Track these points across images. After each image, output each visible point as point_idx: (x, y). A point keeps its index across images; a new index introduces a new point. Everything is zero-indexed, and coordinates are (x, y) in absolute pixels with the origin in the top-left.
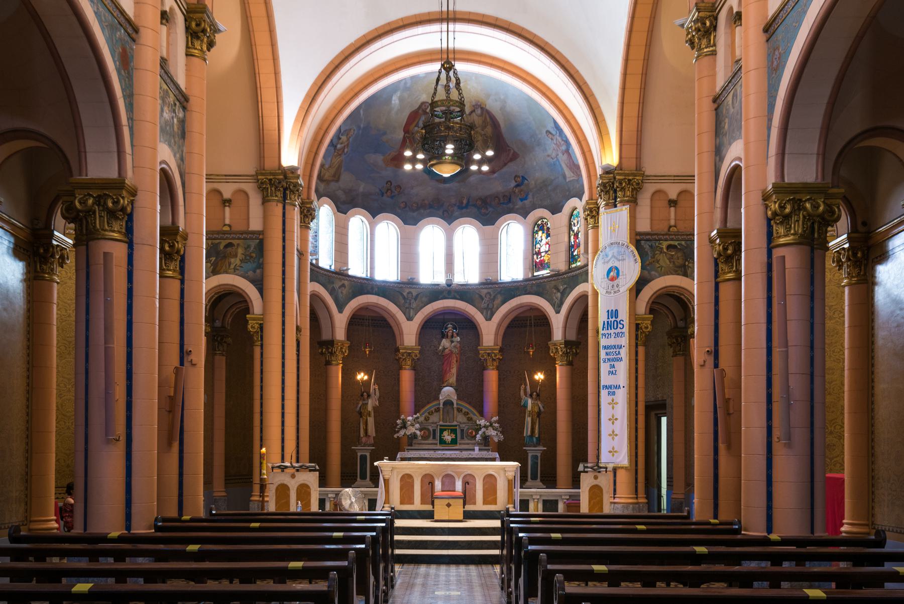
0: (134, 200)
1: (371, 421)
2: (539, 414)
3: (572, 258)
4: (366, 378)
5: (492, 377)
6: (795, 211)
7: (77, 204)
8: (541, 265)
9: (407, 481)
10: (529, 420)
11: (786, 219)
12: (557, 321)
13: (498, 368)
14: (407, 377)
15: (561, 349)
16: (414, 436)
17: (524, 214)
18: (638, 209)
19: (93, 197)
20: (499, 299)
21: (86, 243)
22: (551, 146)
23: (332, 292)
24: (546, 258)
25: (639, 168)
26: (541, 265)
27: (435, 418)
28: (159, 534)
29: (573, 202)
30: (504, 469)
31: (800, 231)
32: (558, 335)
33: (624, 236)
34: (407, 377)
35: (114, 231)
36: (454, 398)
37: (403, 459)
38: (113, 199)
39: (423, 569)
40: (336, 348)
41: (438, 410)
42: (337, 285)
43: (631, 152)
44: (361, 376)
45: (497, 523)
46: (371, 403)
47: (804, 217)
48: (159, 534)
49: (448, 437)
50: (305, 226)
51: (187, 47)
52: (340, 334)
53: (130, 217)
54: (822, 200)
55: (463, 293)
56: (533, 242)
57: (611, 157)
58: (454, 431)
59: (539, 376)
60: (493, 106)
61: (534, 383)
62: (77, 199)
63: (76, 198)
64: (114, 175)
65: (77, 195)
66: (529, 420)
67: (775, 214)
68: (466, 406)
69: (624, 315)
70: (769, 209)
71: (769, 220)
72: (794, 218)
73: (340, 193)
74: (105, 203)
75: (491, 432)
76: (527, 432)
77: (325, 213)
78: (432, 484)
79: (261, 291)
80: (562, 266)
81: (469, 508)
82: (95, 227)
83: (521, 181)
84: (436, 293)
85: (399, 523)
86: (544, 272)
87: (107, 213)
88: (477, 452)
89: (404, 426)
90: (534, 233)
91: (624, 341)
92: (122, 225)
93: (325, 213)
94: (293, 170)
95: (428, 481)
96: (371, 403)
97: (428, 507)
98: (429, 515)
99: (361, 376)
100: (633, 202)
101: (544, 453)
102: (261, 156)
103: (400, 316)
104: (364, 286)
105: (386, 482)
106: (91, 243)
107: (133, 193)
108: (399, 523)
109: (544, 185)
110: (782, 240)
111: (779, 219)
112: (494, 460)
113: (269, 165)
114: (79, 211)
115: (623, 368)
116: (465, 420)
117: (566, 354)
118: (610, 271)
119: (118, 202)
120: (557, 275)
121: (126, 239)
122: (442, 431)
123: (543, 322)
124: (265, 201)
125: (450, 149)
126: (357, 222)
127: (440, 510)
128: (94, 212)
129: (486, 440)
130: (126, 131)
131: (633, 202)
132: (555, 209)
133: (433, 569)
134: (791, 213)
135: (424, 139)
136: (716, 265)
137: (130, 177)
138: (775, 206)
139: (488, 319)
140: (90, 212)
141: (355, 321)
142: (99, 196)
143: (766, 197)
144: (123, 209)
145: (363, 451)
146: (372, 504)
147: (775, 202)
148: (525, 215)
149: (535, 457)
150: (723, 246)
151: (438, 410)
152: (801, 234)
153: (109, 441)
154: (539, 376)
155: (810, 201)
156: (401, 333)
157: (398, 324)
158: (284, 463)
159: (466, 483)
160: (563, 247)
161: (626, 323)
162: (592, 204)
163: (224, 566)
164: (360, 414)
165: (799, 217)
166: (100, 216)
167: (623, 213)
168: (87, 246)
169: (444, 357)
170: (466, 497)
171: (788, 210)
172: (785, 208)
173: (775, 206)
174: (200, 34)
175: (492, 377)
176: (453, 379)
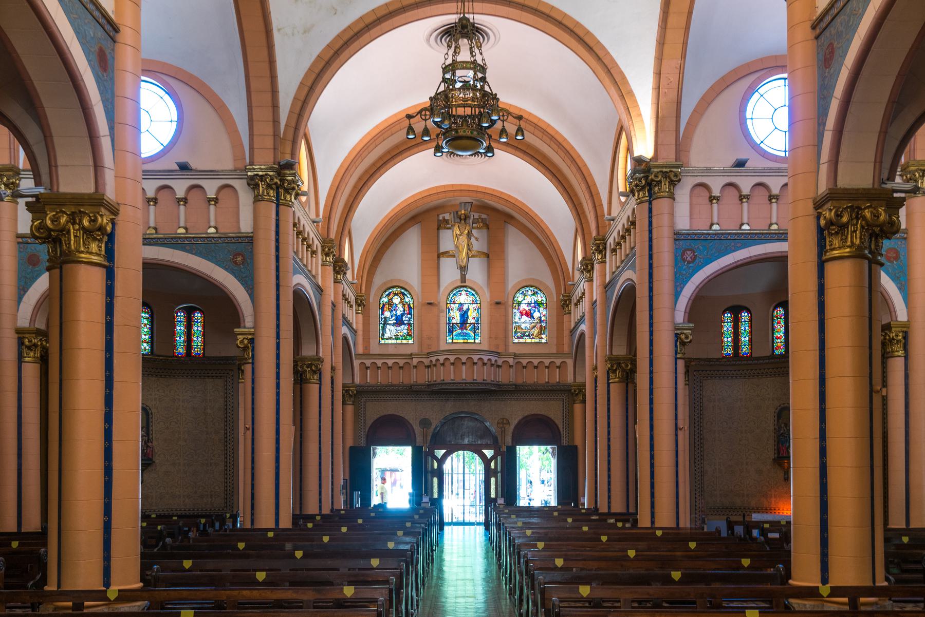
0: (115, 219)
6: (852, 220)
7: (299, 368)
11: (614, 371)
19: (67, 214)
21: (59, 266)
31: (857, 243)
35: (91, 253)
38: (90, 217)
47: (862, 227)
51: (334, 279)
53: (111, 237)
54: (883, 208)
62: (49, 216)
63: (47, 215)
65: (48, 212)
67: (830, 223)
70: (822, 218)
71: (820, 231)
72: (851, 228)
74: (81, 222)
82: (69, 247)
87: (84, 233)
92: (101, 247)
106: (66, 267)
107: (114, 211)
110: (836, 253)
111: (834, 229)
114: (50, 230)
118: (507, 420)
119: (95, 220)
121: (106, 263)
128: (69, 232)
130: (105, 143)
134: (848, 222)
136: (608, 374)
137: (110, 193)
138: (830, 214)
140: (64, 231)
142: (73, 213)
143: (818, 205)
144: (101, 229)
147: (831, 210)
150: (836, 212)
152: (858, 246)
155: (870, 209)
162: (599, 239)
165: (857, 228)
166: (75, 236)
168: (61, 268)
171: (845, 219)
172: (842, 217)
173: (830, 214)
174: (290, 191)
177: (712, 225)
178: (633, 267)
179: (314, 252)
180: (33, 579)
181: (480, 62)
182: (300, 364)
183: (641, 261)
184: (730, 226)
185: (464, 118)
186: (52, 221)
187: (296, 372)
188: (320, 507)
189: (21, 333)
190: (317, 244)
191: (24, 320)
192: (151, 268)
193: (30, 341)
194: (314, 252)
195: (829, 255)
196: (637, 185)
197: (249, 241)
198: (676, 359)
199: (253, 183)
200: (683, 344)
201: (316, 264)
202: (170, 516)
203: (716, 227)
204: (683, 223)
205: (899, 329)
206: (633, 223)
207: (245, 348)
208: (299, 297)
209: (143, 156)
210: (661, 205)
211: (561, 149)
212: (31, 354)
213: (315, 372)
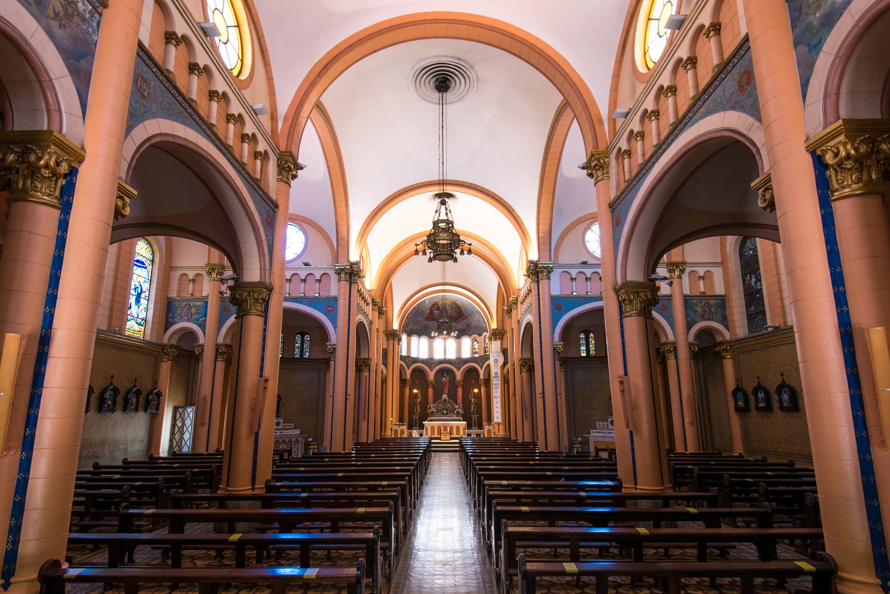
1: (418, 406)
2: (476, 403)
3: (486, 352)
4: (417, 391)
5: (460, 390)
8: (476, 353)
9: (433, 428)
10: (472, 406)
12: (481, 372)
13: (462, 387)
14: (430, 391)
15: (483, 381)
16: (433, 411)
17: (470, 336)
18: (504, 341)
20: (462, 364)
22: (477, 315)
23: (406, 363)
24: (477, 350)
25: (503, 329)
26: (476, 353)
27: (440, 405)
28: (125, 465)
29: (485, 333)
30: (462, 424)
32: (482, 377)
33: (499, 350)
34: (430, 391)
36: (447, 399)
37: (430, 421)
39: (438, 453)
40: (407, 382)
41: (441, 402)
42: (407, 360)
43: (501, 324)
44: (415, 391)
45: (458, 441)
46: (419, 400)
47: (640, 301)
48: (125, 465)
49: (445, 412)
50: (399, 344)
52: (408, 377)
55: (449, 362)
56: (473, 345)
57: (494, 326)
58: (447, 410)
59: (476, 391)
60: (458, 302)
61: (474, 393)
64: (367, 357)
66: (472, 406)
68: (451, 401)
69: (499, 374)
71: (620, 303)
73: (409, 331)
75: (460, 410)
76: (472, 410)
77: (404, 337)
78: (440, 429)
79: (386, 367)
80: (483, 354)
81: (452, 436)
83: (469, 325)
84: (441, 362)
85: (433, 441)
86: (477, 356)
88: (455, 417)
89: (430, 408)
90: (473, 342)
91: (499, 382)
93: (404, 337)
94: (396, 330)
95: (439, 428)
96: (419, 400)
97: (439, 436)
98: (440, 439)
99: (415, 391)
100: (502, 339)
101: (478, 417)
102: (387, 326)
103: (428, 370)
104: (416, 360)
105: (426, 429)
106: (361, 373)
108: (433, 441)
109: (476, 327)
112: (460, 420)
113: (389, 329)
114: (238, 300)
115: (499, 391)
116: (451, 406)
117: (485, 383)
120: (481, 357)
122: (443, 410)
123: (476, 371)
124: (388, 340)
125: (445, 332)
126: (414, 339)
127: (443, 437)
128: (247, 301)
129: (458, 413)
131: (502, 339)
132: (480, 335)
133: (441, 453)
135: (438, 328)
139: (458, 370)
140: (361, 365)
141: (414, 371)
142: (249, 292)
145: (416, 417)
146: (421, 435)
148: (470, 336)
149: (475, 419)
151: (441, 402)
153: (364, 420)
154: (476, 391)
156: (429, 376)
157: (428, 373)
158: (668, 507)
159: (450, 429)
160: (483, 348)
161: (500, 376)
163: (178, 512)
164: (415, 404)
167: (499, 342)
169: (443, 384)
170: (451, 433)
175: (460, 390)
176: (446, 392)
177: (573, 292)
178: (530, 313)
179: (368, 304)
180: (192, 471)
181: (450, 219)
182: (359, 361)
183: (535, 310)
184: (582, 293)
185: (443, 244)
186: (239, 295)
187: (357, 365)
188: (368, 439)
189: (218, 347)
190: (370, 300)
191: (220, 340)
192: (287, 312)
193: (222, 350)
194: (368, 304)
195: (625, 315)
196: (531, 273)
197: (335, 299)
198: (555, 360)
199: (338, 272)
200: (558, 353)
201: (369, 310)
202: (496, 575)
203: (574, 294)
204: (556, 291)
205: (671, 345)
206: (530, 291)
207: (332, 353)
208: (361, 325)
209: (286, 260)
210: (543, 283)
211: (580, 101)
212: (222, 356)
213: (366, 366)
